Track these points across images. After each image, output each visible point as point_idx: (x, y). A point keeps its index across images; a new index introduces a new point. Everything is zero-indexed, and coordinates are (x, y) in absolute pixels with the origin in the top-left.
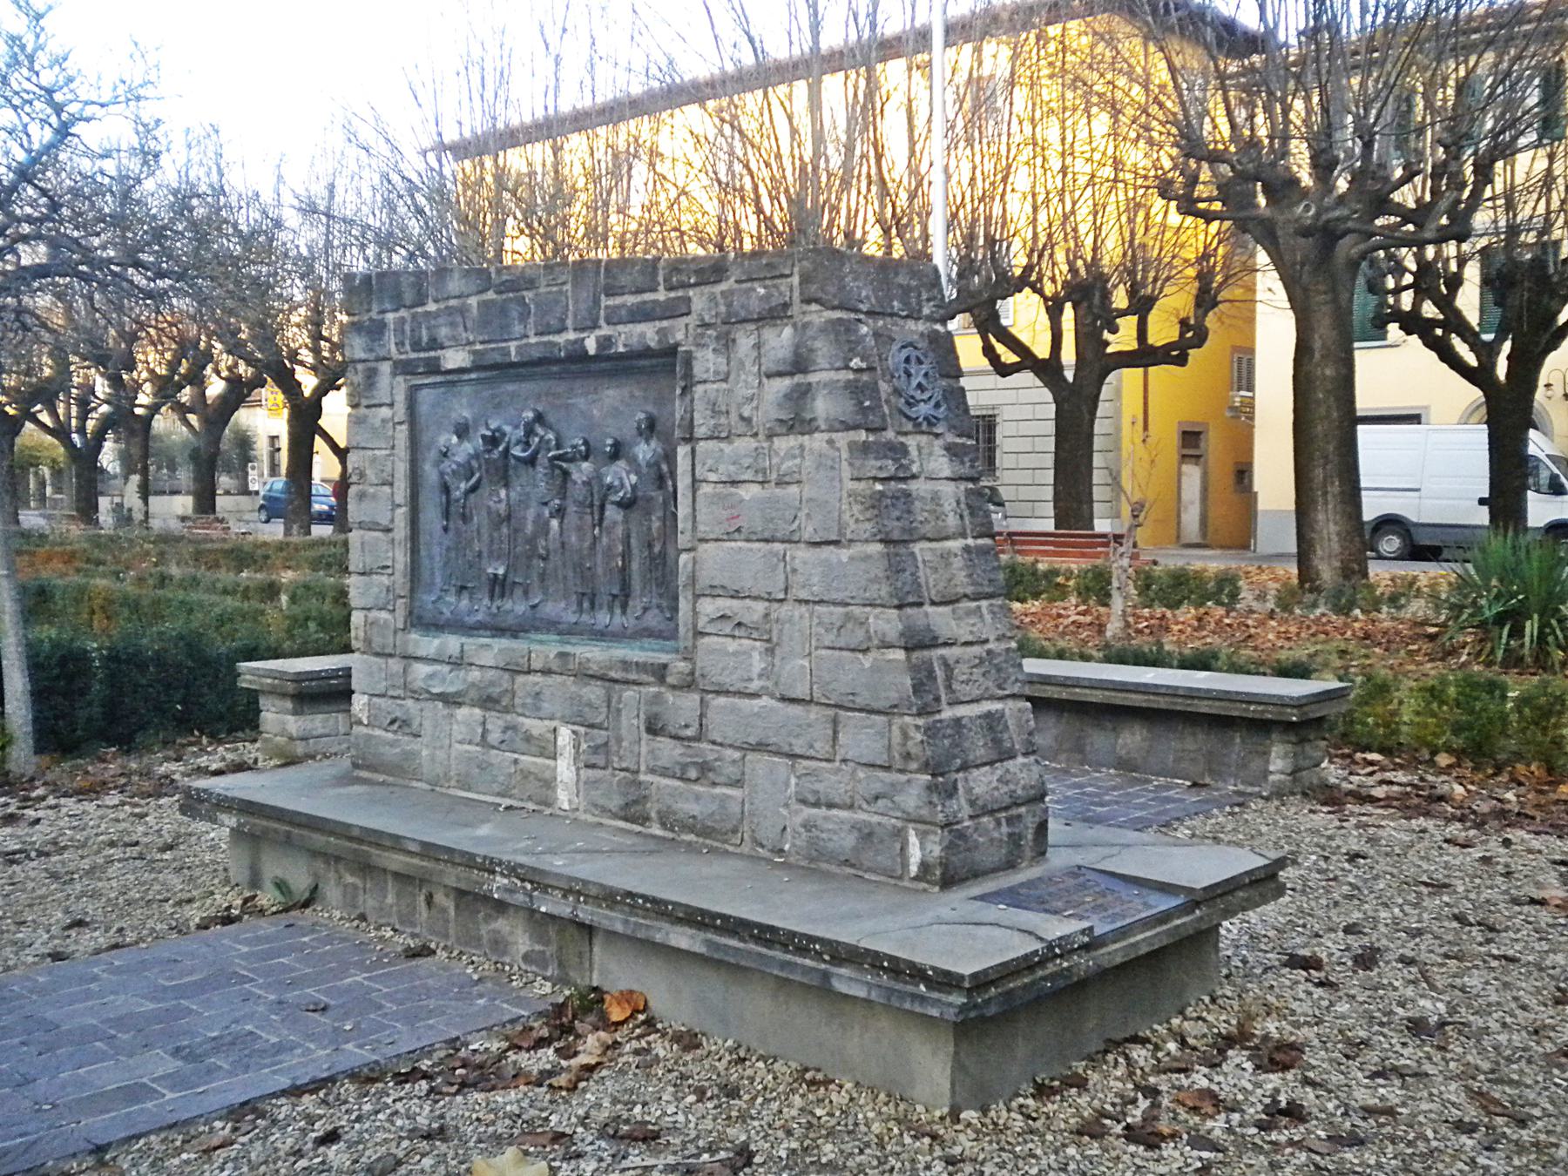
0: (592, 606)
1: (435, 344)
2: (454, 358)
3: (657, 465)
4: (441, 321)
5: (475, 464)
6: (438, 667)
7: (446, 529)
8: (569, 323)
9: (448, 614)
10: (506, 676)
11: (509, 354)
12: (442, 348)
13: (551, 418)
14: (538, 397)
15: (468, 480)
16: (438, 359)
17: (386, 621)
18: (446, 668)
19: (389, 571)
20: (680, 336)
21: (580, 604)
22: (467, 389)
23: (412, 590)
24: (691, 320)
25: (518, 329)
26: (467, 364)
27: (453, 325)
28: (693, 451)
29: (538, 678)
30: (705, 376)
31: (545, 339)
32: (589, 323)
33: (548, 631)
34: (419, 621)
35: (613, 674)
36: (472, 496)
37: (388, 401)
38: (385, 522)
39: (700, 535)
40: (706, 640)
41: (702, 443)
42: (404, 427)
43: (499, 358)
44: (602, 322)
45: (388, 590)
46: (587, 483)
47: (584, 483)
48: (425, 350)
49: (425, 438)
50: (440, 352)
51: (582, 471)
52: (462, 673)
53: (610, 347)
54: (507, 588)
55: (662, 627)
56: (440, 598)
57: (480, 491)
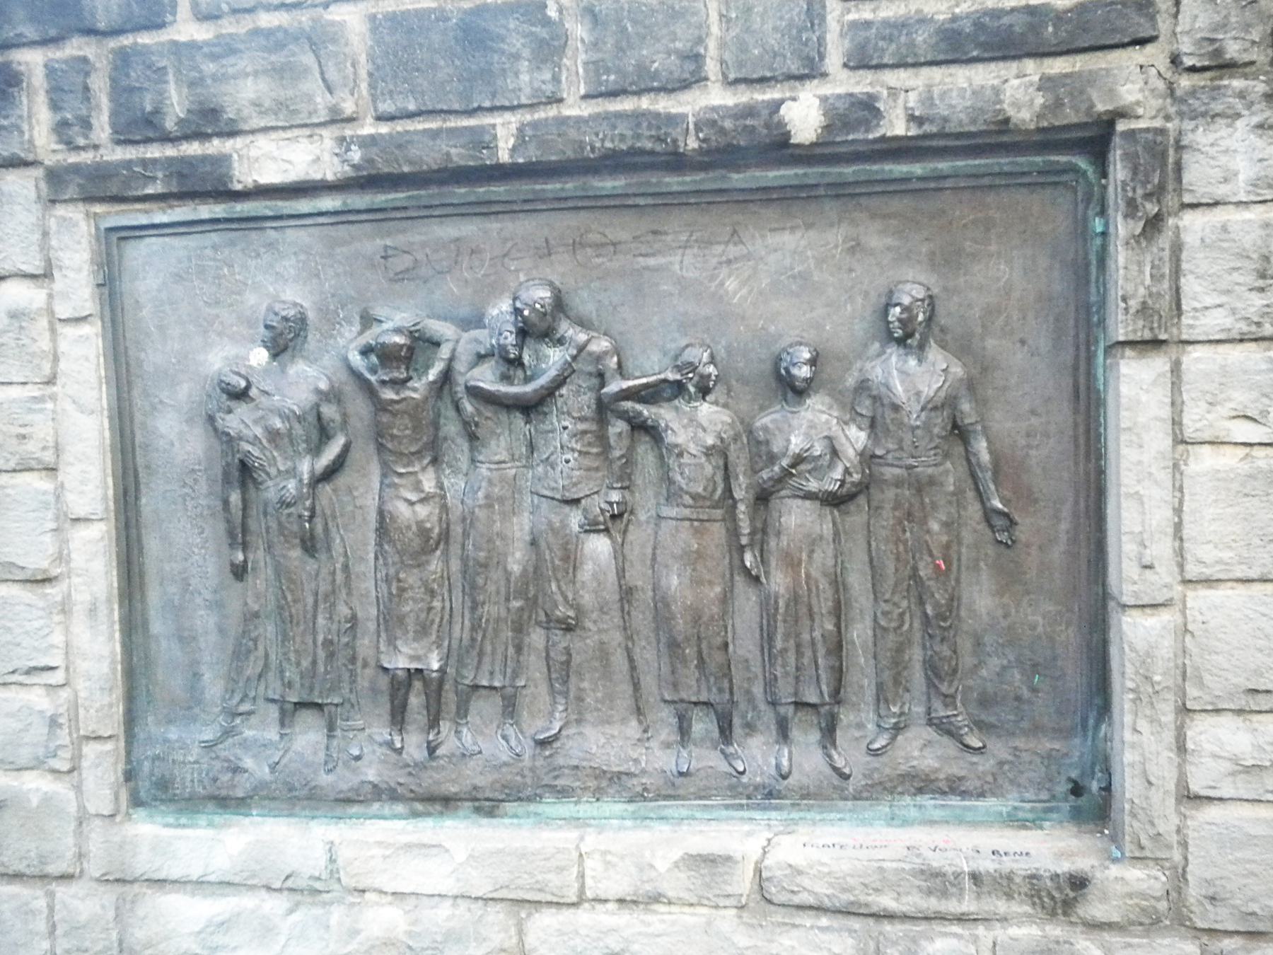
0: (726, 732)
1: (209, 121)
2: (268, 159)
3: (950, 402)
4: (243, 63)
5: (329, 411)
6: (247, 901)
7: (239, 572)
8: (712, 67)
9: (264, 772)
10: (496, 915)
11: (491, 146)
12: (233, 134)
13: (583, 302)
14: (546, 251)
15: (316, 451)
16: (1090, 79)
17: (47, 799)
18: (274, 905)
19: (57, 677)
20: (1129, 93)
21: (684, 731)
22: (296, 236)
23: (131, 720)
24: (1155, 55)
25: (526, 80)
26: (330, 170)
27: (282, 72)
28: (1176, 368)
29: (607, 917)
30: (1221, 191)
31: (626, 105)
32: (794, 67)
33: (598, 794)
34: (150, 787)
35: (887, 902)
36: (326, 489)
37: (35, 266)
38: (37, 560)
39: (1192, 571)
40: (1213, 813)
41: (1196, 352)
42: (92, 331)
43: (459, 155)
44: (834, 60)
45: (53, 723)
46: (719, 452)
47: (709, 452)
48: (167, 139)
49: (153, 357)
50: (215, 146)
51: (696, 426)
52: (337, 915)
53: (867, 125)
54: (450, 697)
55: (956, 770)
56: (228, 733)
57: (342, 480)
